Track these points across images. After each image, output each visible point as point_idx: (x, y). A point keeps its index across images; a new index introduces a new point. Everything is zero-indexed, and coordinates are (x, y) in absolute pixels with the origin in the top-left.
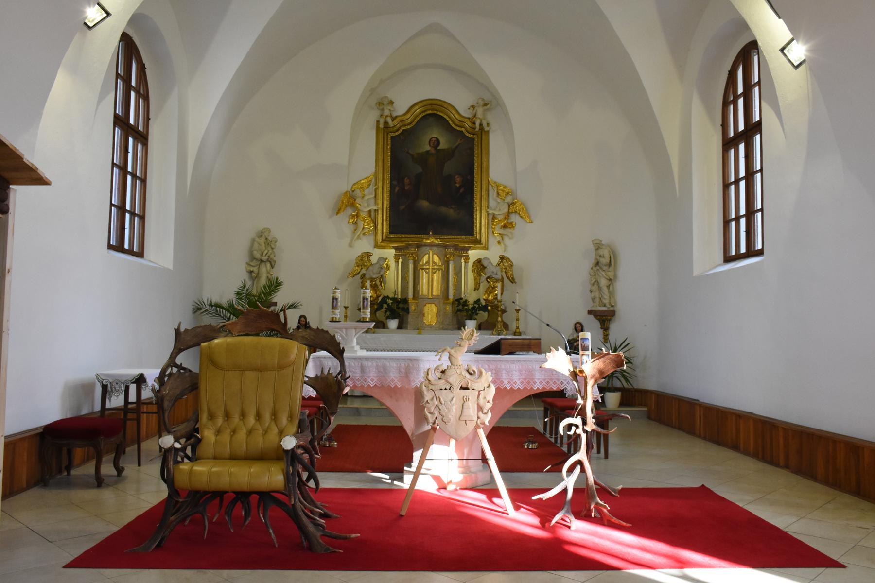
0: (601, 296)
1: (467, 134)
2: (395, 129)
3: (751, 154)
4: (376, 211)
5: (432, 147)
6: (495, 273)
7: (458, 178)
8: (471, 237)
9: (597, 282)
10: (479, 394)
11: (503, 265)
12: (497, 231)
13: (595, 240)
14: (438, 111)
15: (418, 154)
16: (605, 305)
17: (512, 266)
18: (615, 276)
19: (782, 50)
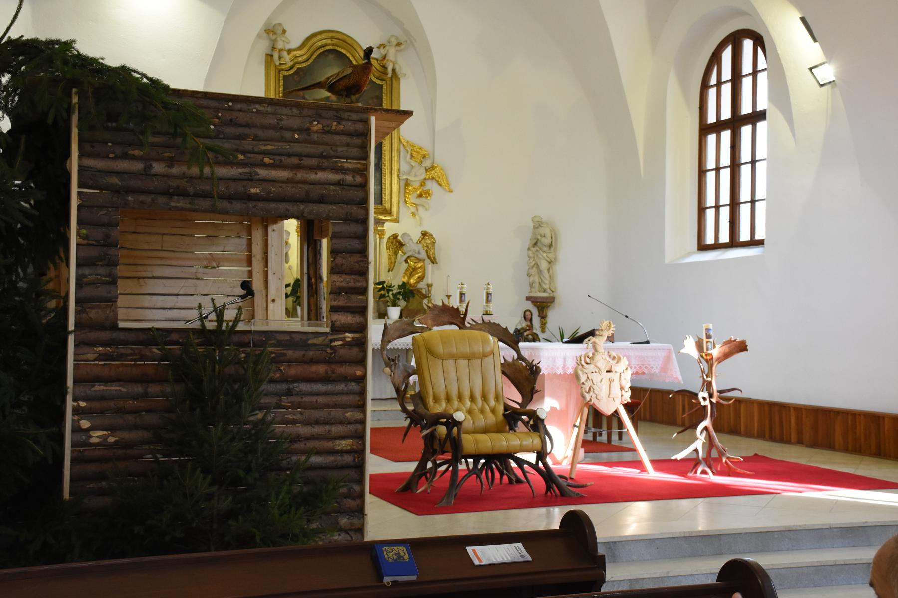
0: (540, 281)
3: (738, 144)
6: (417, 252)
9: (537, 265)
10: (620, 376)
12: (412, 199)
13: (535, 217)
14: (340, 47)
16: (545, 291)
17: (434, 243)
18: (555, 258)
19: (811, 69)
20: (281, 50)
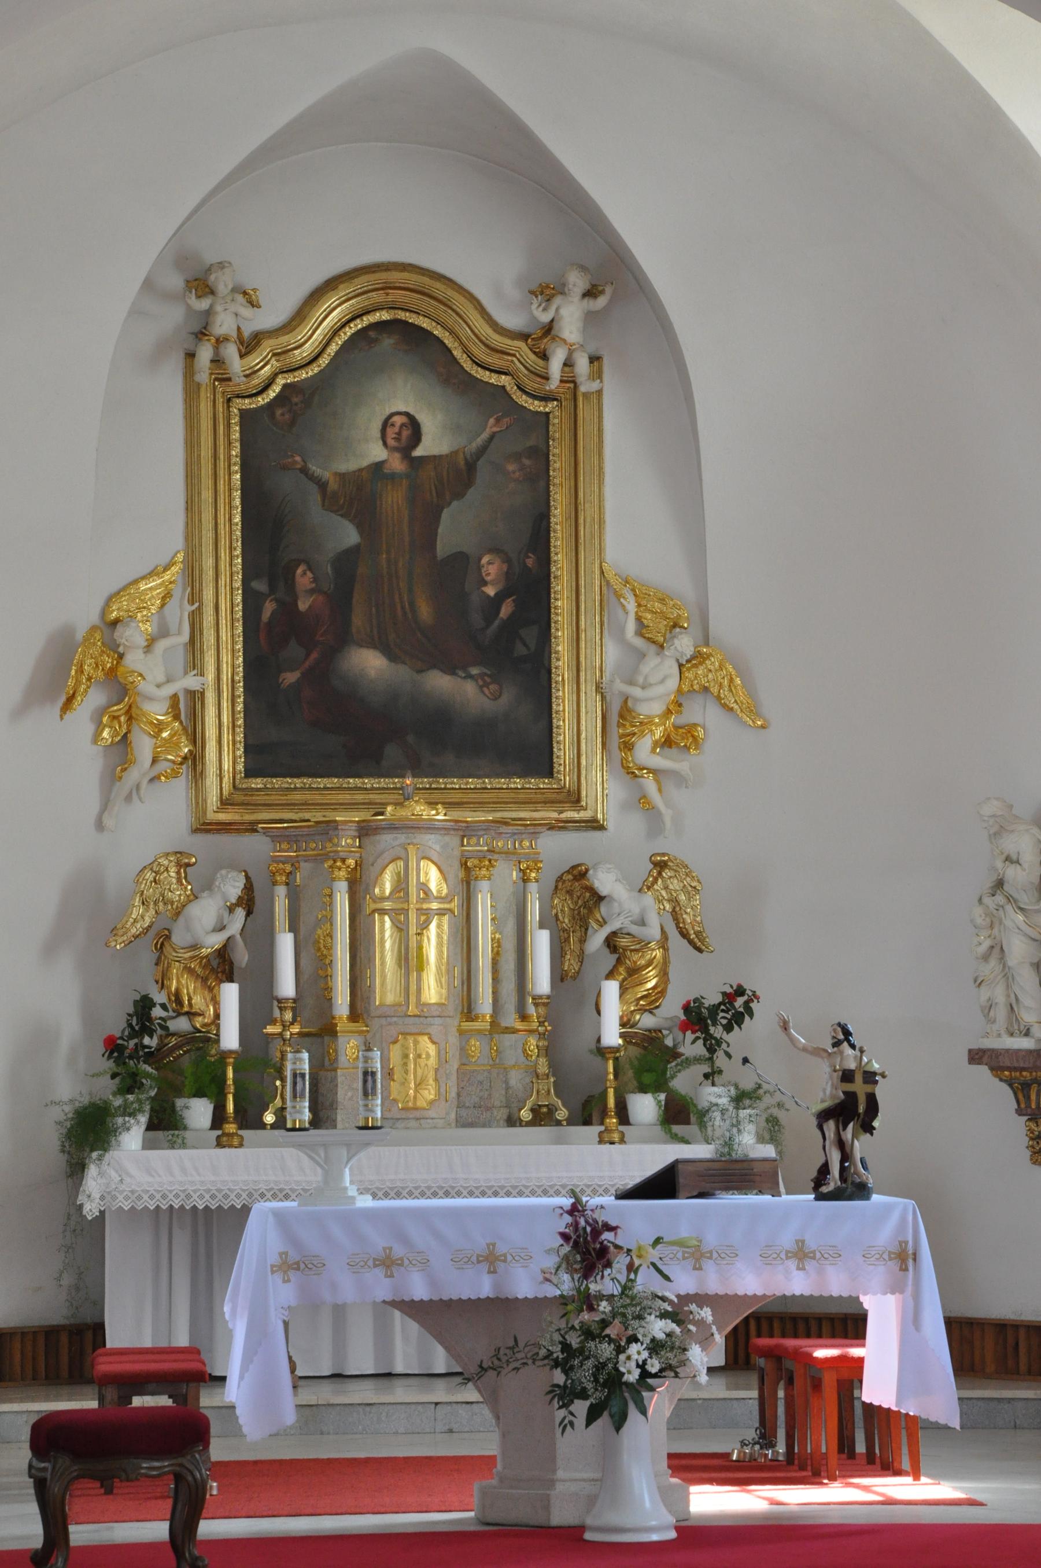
1: (523, 400)
2: (256, 382)
4: (196, 698)
5: (396, 449)
7: (489, 563)
8: (544, 783)
9: (998, 950)
11: (666, 888)
15: (342, 476)
20: (220, 341)
